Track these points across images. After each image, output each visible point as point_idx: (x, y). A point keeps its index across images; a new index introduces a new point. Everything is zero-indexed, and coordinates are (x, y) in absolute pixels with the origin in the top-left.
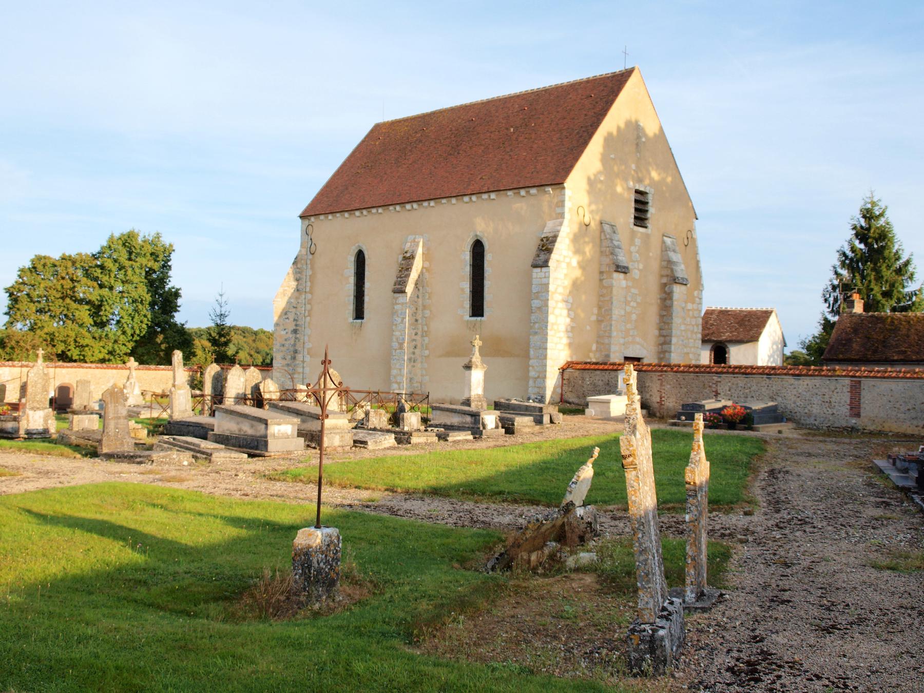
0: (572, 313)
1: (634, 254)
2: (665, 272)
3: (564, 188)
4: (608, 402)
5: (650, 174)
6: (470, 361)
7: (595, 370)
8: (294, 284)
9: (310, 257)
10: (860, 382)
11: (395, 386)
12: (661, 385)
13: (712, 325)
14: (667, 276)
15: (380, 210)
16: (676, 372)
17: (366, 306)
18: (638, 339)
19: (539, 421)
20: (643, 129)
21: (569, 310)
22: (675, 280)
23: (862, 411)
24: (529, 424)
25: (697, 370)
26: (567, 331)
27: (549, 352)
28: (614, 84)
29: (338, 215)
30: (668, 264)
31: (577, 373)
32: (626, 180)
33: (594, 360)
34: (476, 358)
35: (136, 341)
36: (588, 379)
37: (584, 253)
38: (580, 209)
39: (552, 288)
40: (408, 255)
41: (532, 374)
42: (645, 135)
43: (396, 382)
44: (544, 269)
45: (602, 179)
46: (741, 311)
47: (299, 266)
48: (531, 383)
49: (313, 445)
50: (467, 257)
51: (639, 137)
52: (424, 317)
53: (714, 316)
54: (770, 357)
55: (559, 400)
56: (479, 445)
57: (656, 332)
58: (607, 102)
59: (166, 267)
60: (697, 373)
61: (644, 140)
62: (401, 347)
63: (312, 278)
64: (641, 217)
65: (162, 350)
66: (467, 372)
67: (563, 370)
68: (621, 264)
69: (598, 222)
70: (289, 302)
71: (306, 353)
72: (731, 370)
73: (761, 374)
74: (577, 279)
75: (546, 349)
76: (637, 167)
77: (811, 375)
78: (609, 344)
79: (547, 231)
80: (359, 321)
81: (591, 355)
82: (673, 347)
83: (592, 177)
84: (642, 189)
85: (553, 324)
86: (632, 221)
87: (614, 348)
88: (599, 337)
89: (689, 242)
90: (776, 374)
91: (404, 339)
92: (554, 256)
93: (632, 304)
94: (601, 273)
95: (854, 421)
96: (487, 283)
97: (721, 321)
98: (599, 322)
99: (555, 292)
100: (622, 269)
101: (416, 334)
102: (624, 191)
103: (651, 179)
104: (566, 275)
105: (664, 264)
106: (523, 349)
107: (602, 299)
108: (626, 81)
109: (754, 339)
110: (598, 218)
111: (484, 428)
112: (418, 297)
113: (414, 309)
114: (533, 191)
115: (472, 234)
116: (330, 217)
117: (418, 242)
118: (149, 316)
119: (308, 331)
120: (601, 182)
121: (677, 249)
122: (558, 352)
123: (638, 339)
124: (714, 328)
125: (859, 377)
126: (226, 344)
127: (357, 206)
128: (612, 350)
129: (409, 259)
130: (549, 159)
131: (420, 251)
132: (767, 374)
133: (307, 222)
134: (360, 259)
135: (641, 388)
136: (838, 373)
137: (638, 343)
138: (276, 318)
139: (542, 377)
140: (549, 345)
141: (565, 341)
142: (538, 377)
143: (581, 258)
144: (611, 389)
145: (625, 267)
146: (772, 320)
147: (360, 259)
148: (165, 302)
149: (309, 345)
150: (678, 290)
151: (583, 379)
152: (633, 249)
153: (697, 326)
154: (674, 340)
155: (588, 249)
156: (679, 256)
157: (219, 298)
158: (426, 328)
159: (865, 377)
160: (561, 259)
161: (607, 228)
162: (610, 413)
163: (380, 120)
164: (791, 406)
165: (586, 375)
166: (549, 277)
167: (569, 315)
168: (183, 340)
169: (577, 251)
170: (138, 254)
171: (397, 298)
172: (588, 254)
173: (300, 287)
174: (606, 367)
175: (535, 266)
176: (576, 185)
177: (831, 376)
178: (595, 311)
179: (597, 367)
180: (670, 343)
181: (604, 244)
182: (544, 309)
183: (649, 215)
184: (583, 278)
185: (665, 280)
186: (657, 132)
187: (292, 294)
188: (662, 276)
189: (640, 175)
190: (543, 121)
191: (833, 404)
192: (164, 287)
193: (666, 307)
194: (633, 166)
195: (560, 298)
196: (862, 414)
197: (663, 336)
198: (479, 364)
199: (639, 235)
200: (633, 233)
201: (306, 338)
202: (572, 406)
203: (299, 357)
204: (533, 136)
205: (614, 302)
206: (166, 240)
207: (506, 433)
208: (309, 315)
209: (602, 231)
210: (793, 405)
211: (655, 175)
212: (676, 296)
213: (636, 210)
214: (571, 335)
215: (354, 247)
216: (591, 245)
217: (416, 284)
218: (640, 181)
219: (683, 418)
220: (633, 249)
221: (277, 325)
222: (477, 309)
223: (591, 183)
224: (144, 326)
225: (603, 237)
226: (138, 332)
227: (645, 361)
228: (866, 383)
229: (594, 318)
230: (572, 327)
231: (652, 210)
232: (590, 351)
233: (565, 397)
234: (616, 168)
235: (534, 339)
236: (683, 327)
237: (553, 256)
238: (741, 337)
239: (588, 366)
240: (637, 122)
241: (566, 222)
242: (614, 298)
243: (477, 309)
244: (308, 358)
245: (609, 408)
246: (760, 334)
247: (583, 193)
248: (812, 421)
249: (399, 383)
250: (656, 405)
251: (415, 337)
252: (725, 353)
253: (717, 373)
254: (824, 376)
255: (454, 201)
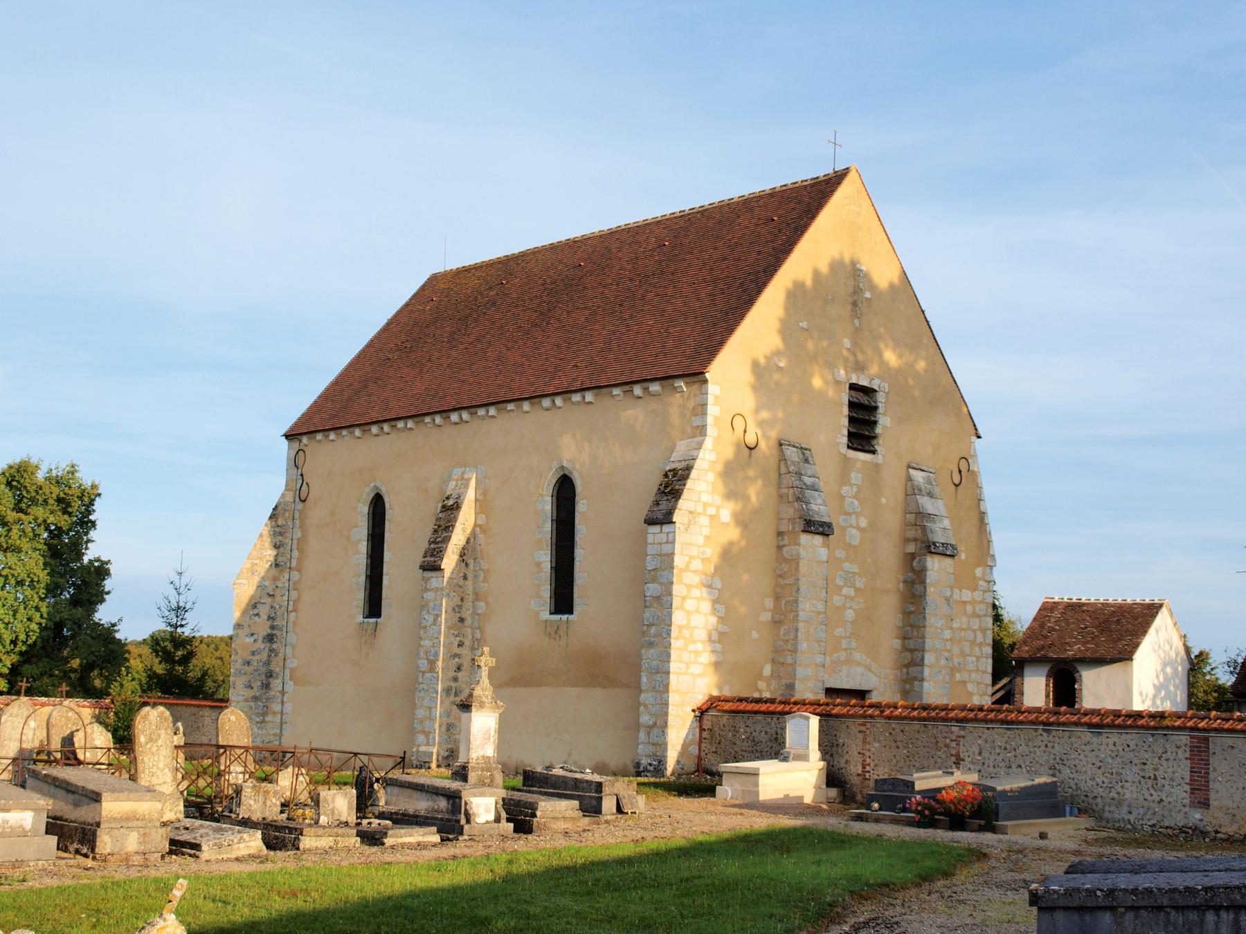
0: (721, 608)
1: (848, 500)
2: (911, 534)
3: (706, 381)
4: (755, 774)
5: (880, 355)
6: (471, 695)
7: (756, 712)
8: (270, 553)
9: (300, 506)
10: (1207, 739)
11: (421, 738)
12: (864, 742)
13: (1051, 630)
14: (915, 540)
15: (410, 424)
16: (889, 718)
17: (385, 593)
18: (858, 656)
19: (592, 808)
20: (867, 276)
21: (714, 602)
22: (930, 548)
23: (1212, 796)
24: (569, 813)
25: (924, 714)
26: (710, 640)
27: (673, 678)
28: (811, 198)
29: (344, 432)
30: (918, 520)
31: (725, 719)
32: (831, 366)
33: (767, 695)
34: (484, 689)
35: (21, 653)
36: (743, 726)
37: (746, 498)
38: (738, 420)
39: (679, 561)
40: (451, 502)
41: (645, 719)
42: (872, 287)
43: (423, 732)
44: (666, 528)
45: (782, 365)
46: (1106, 605)
47: (280, 522)
48: (642, 736)
49: (85, 851)
50: (546, 505)
51: (857, 291)
52: (475, 613)
53: (1057, 614)
54: (1158, 689)
55: (693, 767)
56: (459, 847)
57: (897, 643)
58: (796, 230)
59: (86, 523)
60: (924, 719)
61: (868, 295)
62: (432, 668)
63: (302, 542)
64: (862, 426)
65: (75, 671)
66: (464, 715)
67: (701, 713)
68: (817, 518)
69: (773, 442)
70: (260, 587)
71: (287, 678)
72: (981, 715)
73: (1031, 723)
74: (731, 544)
75: (668, 673)
76: (855, 343)
77: (1120, 727)
78: (794, 665)
79: (676, 460)
80: (373, 620)
81: (762, 684)
82: (927, 671)
83: (762, 361)
84: (864, 382)
85: (681, 628)
86: (845, 440)
87: (801, 672)
88: (776, 651)
89: (964, 477)
90: (1059, 724)
91: (437, 654)
92: (683, 504)
93: (845, 591)
94: (780, 534)
95: (1198, 816)
96: (579, 553)
97: (1068, 624)
98: (777, 623)
99: (686, 569)
100: (822, 529)
101: (461, 645)
102: (828, 388)
103: (883, 364)
104: (708, 538)
105: (911, 517)
106: (630, 670)
107: (781, 581)
108: (832, 192)
109: (1125, 656)
110: (773, 434)
111: (468, 821)
112: (465, 578)
113: (457, 600)
114: (655, 387)
115: (555, 465)
116: (332, 436)
117: (469, 479)
118: (44, 610)
119: (292, 638)
120: (779, 369)
121: (937, 490)
122: (693, 678)
123: (858, 656)
124: (1055, 635)
125: (1204, 730)
126: (1235, 662)
127: (375, 416)
128: (799, 676)
129: (451, 509)
130: (688, 330)
131: (471, 495)
132: (1044, 724)
133: (296, 445)
134: (378, 507)
135: (829, 748)
136: (1063, 719)
137: (859, 664)
138: (237, 615)
139: (661, 725)
140: (673, 666)
141: (706, 658)
142: (655, 725)
143: (739, 506)
144: (775, 749)
145: (823, 524)
146: (1162, 620)
147: (378, 507)
148: (78, 583)
149: (292, 663)
150: (936, 567)
151: (735, 730)
152: (845, 490)
153: (984, 631)
154: (929, 658)
155: (754, 492)
156: (940, 503)
157: (176, 578)
158: (478, 635)
159: (1215, 730)
160: (700, 509)
161: (791, 453)
162: (757, 793)
163: (439, 269)
164: (1086, 784)
165: (740, 721)
166: (673, 542)
167: (714, 611)
168: (109, 650)
169: (731, 495)
170: (34, 501)
171: (428, 579)
172: (754, 499)
173: (280, 559)
174: (772, 708)
175: (650, 522)
176: (730, 378)
177: (1155, 728)
178: (769, 603)
179: (757, 707)
180: (921, 663)
181: (785, 482)
182: (664, 601)
183: (878, 430)
184: (743, 543)
185: (911, 548)
186: (896, 281)
187: (268, 571)
188: (907, 540)
189: (860, 357)
190: (690, 266)
191: (1161, 782)
192: (80, 556)
193: (914, 596)
194: (847, 343)
195: (696, 579)
196: (1213, 803)
197: (912, 651)
198: (487, 700)
199: (859, 465)
200: (846, 463)
201: (289, 651)
202: (698, 783)
203: (276, 684)
204: (670, 291)
205: (803, 588)
206: (86, 477)
207: (516, 830)
208: (294, 610)
209: (782, 458)
210: (1090, 783)
211: (891, 357)
212: (931, 577)
213: (852, 420)
214: (718, 647)
215: (367, 489)
216: (760, 483)
217: (462, 555)
218: (860, 368)
219: (876, 805)
220: (845, 490)
221: (238, 626)
222: (563, 600)
223: (760, 371)
224: (34, 626)
225: (783, 470)
226: (22, 637)
227: (874, 698)
228: (1218, 743)
229: (766, 616)
230: (721, 634)
231: (884, 421)
232: (760, 677)
233: (706, 763)
234: (810, 345)
235: (649, 655)
236: (947, 634)
237: (682, 503)
238: (1102, 651)
239: (742, 706)
240: (854, 263)
241: (708, 443)
242: (803, 580)
243: (563, 600)
244: (290, 687)
245: (757, 785)
246: (1137, 646)
247: (739, 389)
248: (1122, 814)
249: (427, 734)
250: (855, 780)
251: (458, 651)
252: (1074, 681)
253: (958, 720)
254: (1143, 727)
255: (526, 406)
